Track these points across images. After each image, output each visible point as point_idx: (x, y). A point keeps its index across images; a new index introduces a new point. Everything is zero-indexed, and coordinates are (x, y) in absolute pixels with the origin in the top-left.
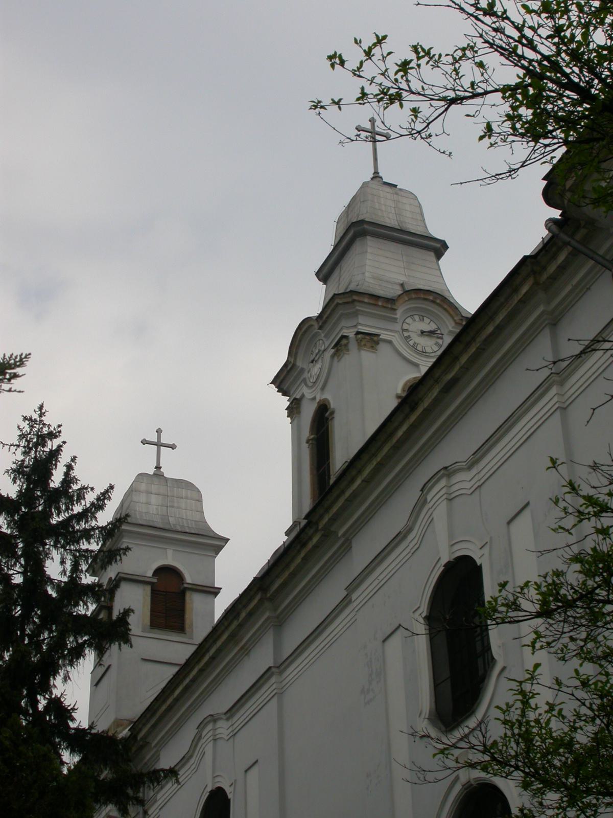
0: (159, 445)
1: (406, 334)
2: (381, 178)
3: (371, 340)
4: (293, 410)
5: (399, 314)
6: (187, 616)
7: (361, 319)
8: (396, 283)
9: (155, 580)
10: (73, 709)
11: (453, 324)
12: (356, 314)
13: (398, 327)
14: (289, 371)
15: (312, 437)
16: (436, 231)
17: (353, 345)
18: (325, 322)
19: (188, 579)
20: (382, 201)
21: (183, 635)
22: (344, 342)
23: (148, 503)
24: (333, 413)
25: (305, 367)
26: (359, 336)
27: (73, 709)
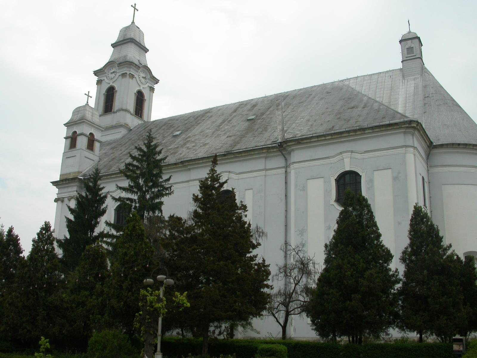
0: (88, 96)
1: (139, 76)
2: (134, 23)
3: (132, 76)
4: (99, 82)
5: (139, 71)
6: (94, 147)
7: (131, 70)
8: (137, 59)
9: (89, 136)
10: (164, 204)
11: (150, 77)
12: (130, 68)
13: (138, 74)
14: (101, 71)
15: (106, 93)
16: (147, 46)
17: (128, 76)
18: (120, 66)
19: (96, 137)
20: (137, 33)
21: (91, 152)
22: (126, 74)
23: (89, 114)
24: (116, 91)
25: (107, 72)
26: (130, 75)
27: (164, 204)
